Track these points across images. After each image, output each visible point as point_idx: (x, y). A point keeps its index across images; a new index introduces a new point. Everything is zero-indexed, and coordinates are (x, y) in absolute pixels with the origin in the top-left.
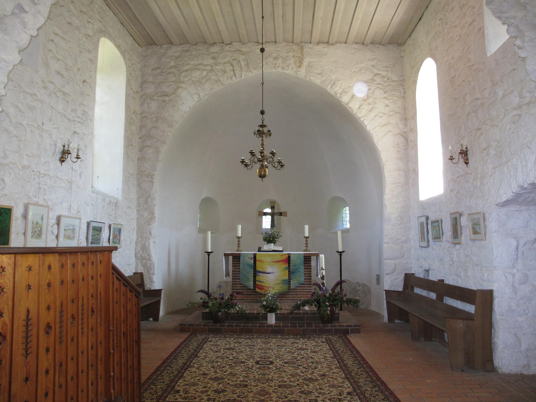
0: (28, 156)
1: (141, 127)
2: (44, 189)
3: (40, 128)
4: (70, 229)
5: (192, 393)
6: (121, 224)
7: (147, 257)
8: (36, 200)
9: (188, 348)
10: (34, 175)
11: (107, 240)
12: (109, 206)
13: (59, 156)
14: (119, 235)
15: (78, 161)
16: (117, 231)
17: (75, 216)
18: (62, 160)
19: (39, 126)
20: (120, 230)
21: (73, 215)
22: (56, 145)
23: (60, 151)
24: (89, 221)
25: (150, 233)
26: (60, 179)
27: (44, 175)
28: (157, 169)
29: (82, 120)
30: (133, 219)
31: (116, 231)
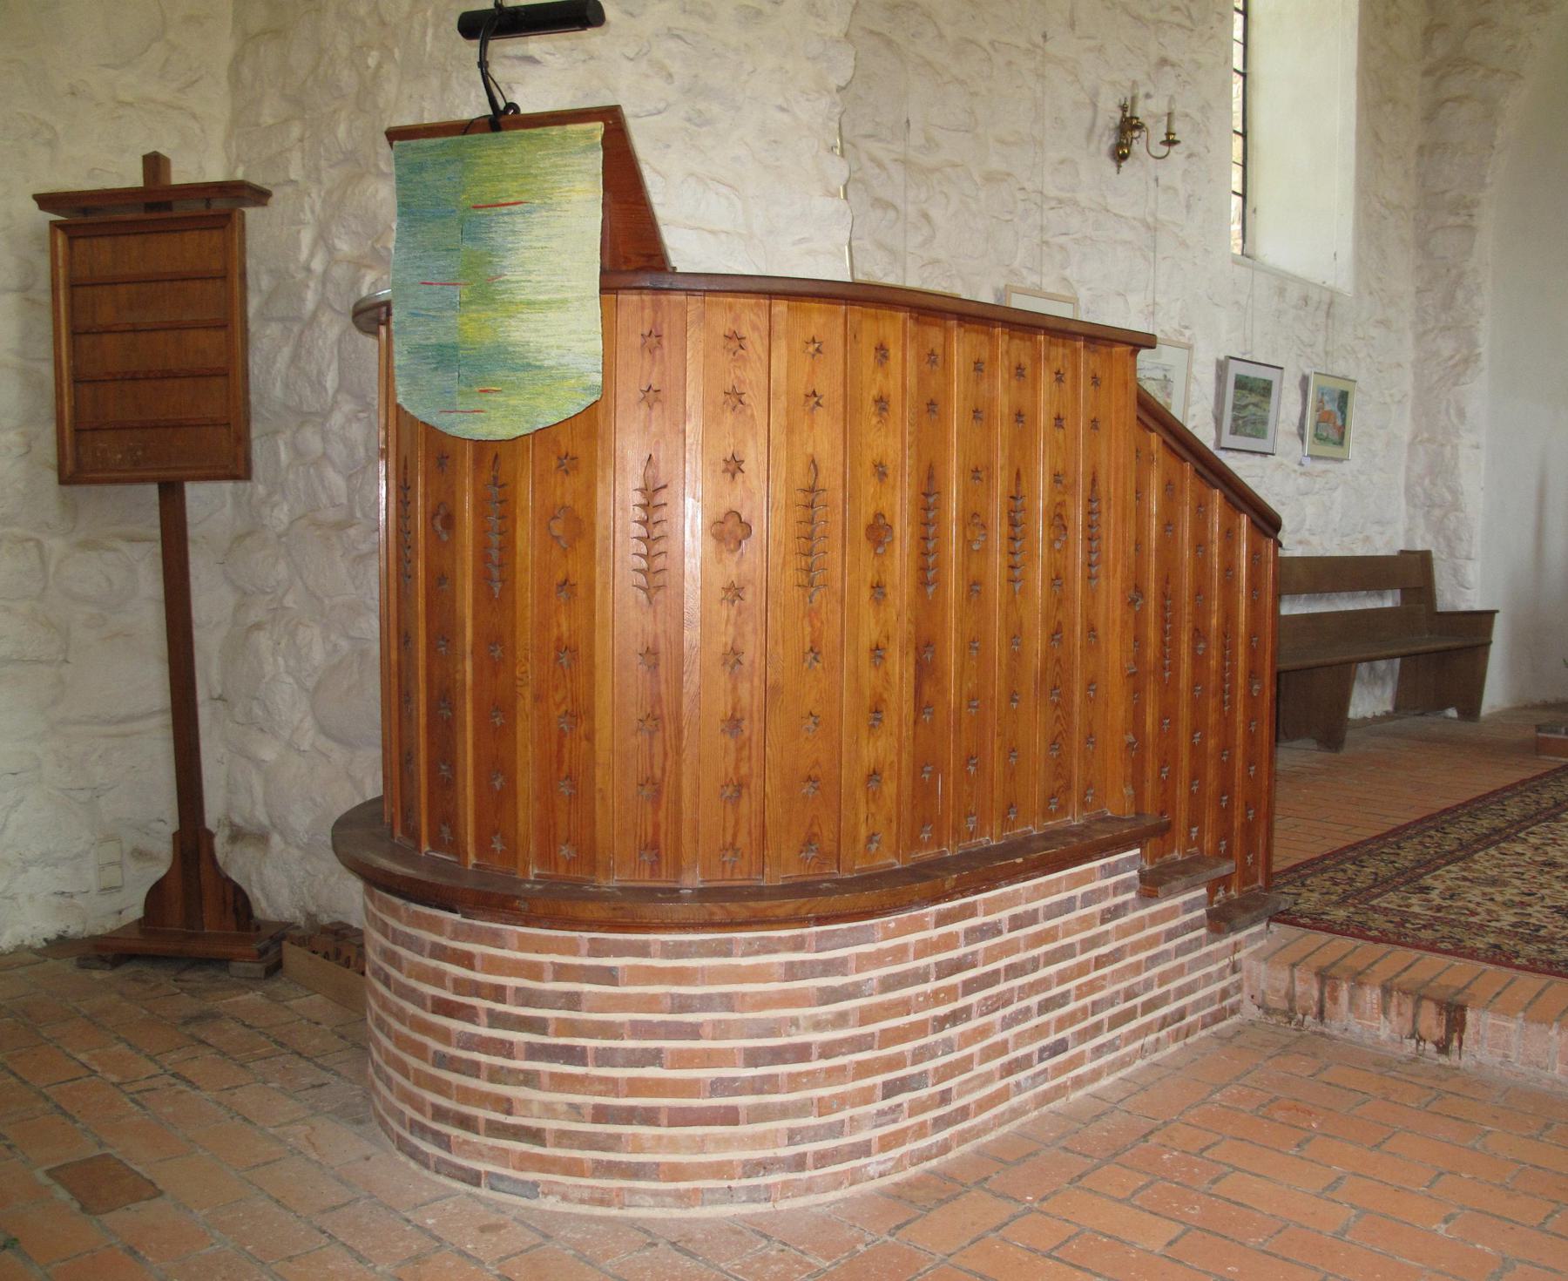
0: (1003, 142)
1: (1429, 33)
2: (1062, 247)
3: (1039, 51)
4: (1154, 379)
5: (1470, 902)
6: (1352, 377)
7: (1448, 497)
8: (1035, 279)
9: (1534, 796)
10: (1023, 200)
11: (1294, 429)
12: (1302, 313)
13: (1109, 141)
14: (1339, 414)
15: (1172, 151)
16: (1332, 400)
17: (1174, 338)
18: (1120, 155)
19: (1036, 46)
20: (1343, 398)
21: (1166, 335)
22: (1095, 105)
23: (1112, 125)
24: (1222, 357)
25: (1461, 414)
26: (1115, 215)
27: (1060, 201)
28: (1488, 180)
29: (1190, 17)
30: (1399, 365)
31: (1326, 398)
